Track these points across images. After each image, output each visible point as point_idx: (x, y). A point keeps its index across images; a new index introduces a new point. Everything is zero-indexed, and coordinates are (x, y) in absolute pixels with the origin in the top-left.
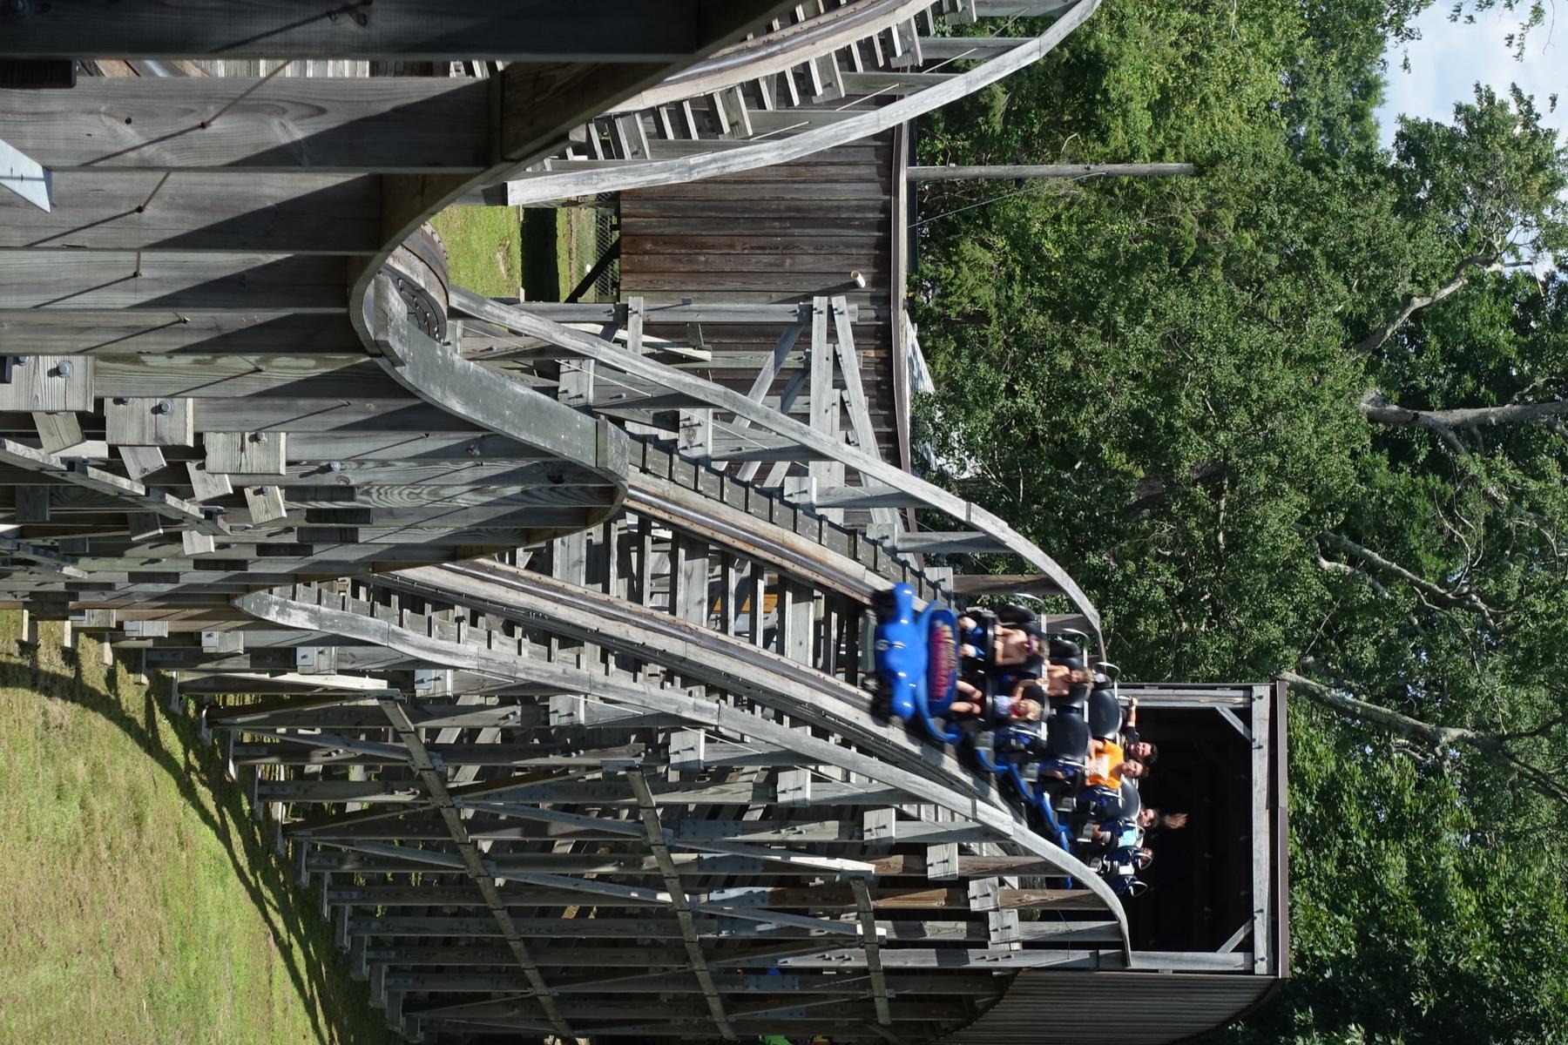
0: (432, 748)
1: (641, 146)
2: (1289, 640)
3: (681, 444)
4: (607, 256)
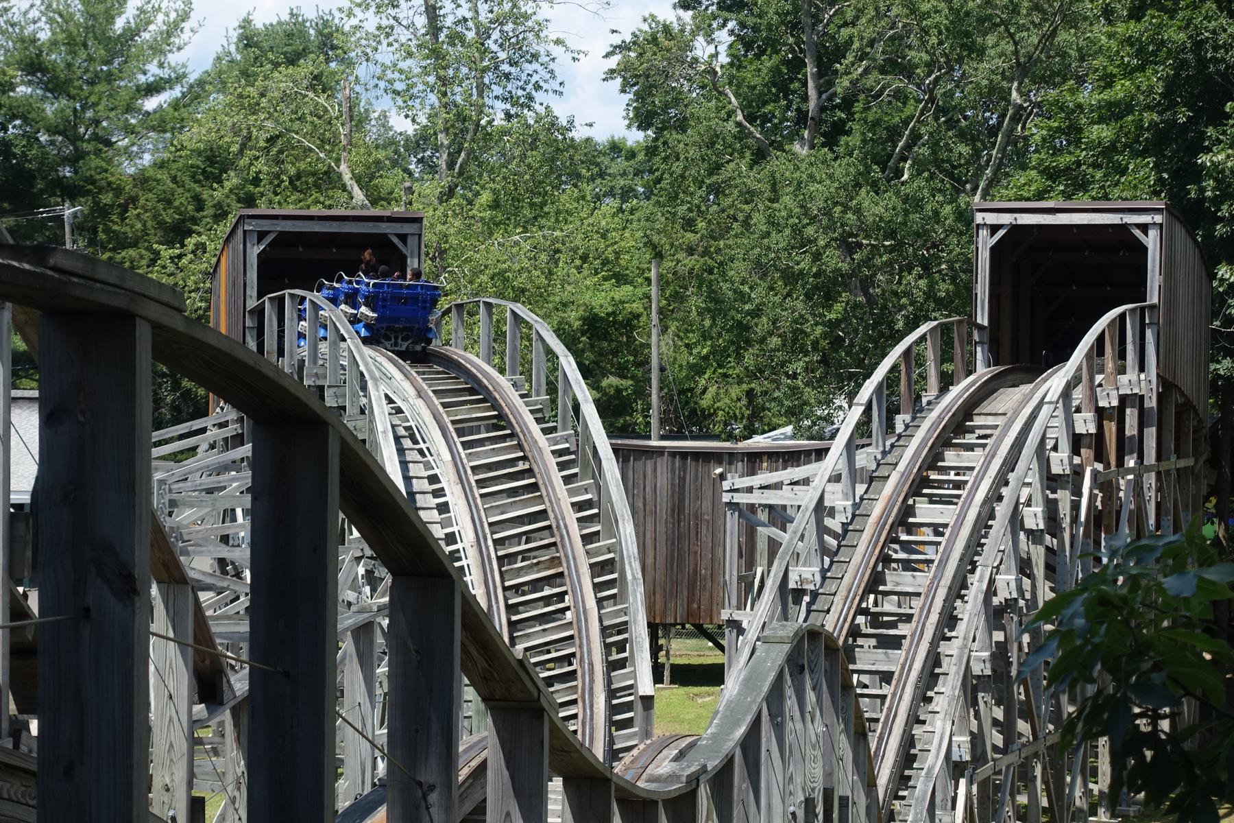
0: (1005, 751)
1: (621, 610)
2: (953, 200)
3: (813, 588)
4: (701, 632)
